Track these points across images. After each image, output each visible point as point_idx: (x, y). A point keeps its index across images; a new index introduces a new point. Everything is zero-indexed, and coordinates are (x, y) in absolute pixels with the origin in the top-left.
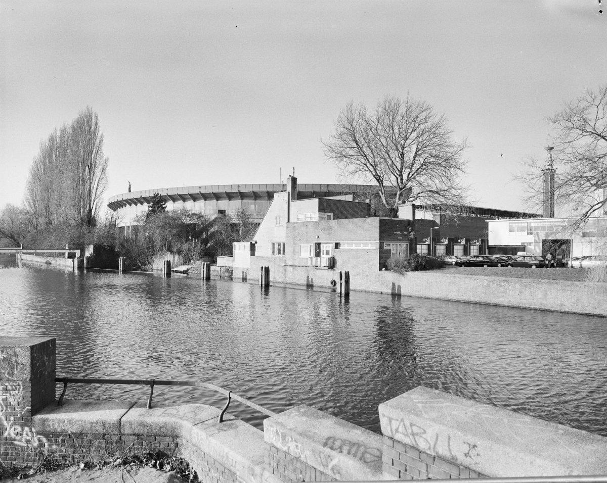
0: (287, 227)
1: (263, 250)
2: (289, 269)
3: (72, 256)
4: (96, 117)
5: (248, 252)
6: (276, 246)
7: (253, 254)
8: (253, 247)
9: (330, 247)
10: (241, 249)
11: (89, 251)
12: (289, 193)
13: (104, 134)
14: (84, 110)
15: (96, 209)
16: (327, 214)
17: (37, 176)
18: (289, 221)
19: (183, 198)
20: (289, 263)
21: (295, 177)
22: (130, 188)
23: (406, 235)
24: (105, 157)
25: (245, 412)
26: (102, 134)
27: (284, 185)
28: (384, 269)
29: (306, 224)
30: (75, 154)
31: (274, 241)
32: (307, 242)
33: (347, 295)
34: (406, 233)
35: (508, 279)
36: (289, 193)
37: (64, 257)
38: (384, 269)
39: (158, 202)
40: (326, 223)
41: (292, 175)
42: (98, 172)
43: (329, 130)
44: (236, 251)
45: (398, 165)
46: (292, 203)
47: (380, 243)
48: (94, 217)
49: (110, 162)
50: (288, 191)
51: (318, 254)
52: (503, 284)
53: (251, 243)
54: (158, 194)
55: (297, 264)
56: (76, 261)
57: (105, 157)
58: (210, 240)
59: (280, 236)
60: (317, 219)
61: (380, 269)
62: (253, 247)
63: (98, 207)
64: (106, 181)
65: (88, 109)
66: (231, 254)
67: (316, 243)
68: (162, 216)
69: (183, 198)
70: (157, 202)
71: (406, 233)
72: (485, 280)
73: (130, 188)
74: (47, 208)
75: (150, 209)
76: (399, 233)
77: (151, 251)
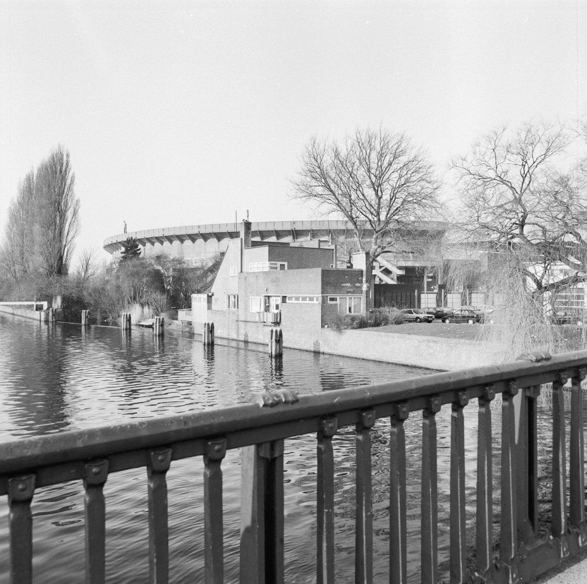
0: (240, 278)
1: (220, 303)
2: (242, 325)
3: (39, 308)
4: (68, 155)
5: (205, 304)
6: (232, 299)
7: (209, 308)
8: (210, 298)
9: (279, 301)
10: (198, 300)
11: (58, 303)
12: (242, 239)
13: (76, 176)
14: (55, 149)
15: (67, 256)
16: (279, 264)
17: (14, 218)
18: (241, 272)
19: (160, 240)
20: (242, 318)
21: (250, 221)
22: (125, 228)
23: (358, 287)
24: (76, 198)
25: (526, 520)
26: (74, 174)
27: (238, 233)
28: (326, 326)
29: (256, 275)
30: (50, 195)
31: (229, 294)
32: (258, 295)
33: (279, 356)
34: (358, 285)
35: (435, 339)
36: (242, 239)
37: (33, 310)
38: (326, 326)
39: (132, 247)
40: (280, 273)
41: (246, 219)
42: (69, 214)
43: (295, 167)
44: (194, 304)
45: (374, 202)
46: (245, 251)
47: (322, 296)
48: (65, 265)
49: (81, 203)
50: (241, 237)
51: (267, 309)
52: (432, 344)
53: (208, 295)
54: (132, 238)
55: (248, 320)
56: (43, 314)
57: (76, 198)
58: (176, 289)
59: (234, 287)
60: (267, 269)
61: (323, 327)
62: (210, 298)
63: (69, 254)
64: (78, 225)
65: (60, 148)
66: (189, 306)
67: (265, 296)
68: (135, 261)
69: (160, 240)
70: (131, 247)
71: (358, 285)
72: (415, 339)
73: (125, 228)
74: (22, 253)
75: (123, 255)
76: (349, 285)
77: (121, 302)
